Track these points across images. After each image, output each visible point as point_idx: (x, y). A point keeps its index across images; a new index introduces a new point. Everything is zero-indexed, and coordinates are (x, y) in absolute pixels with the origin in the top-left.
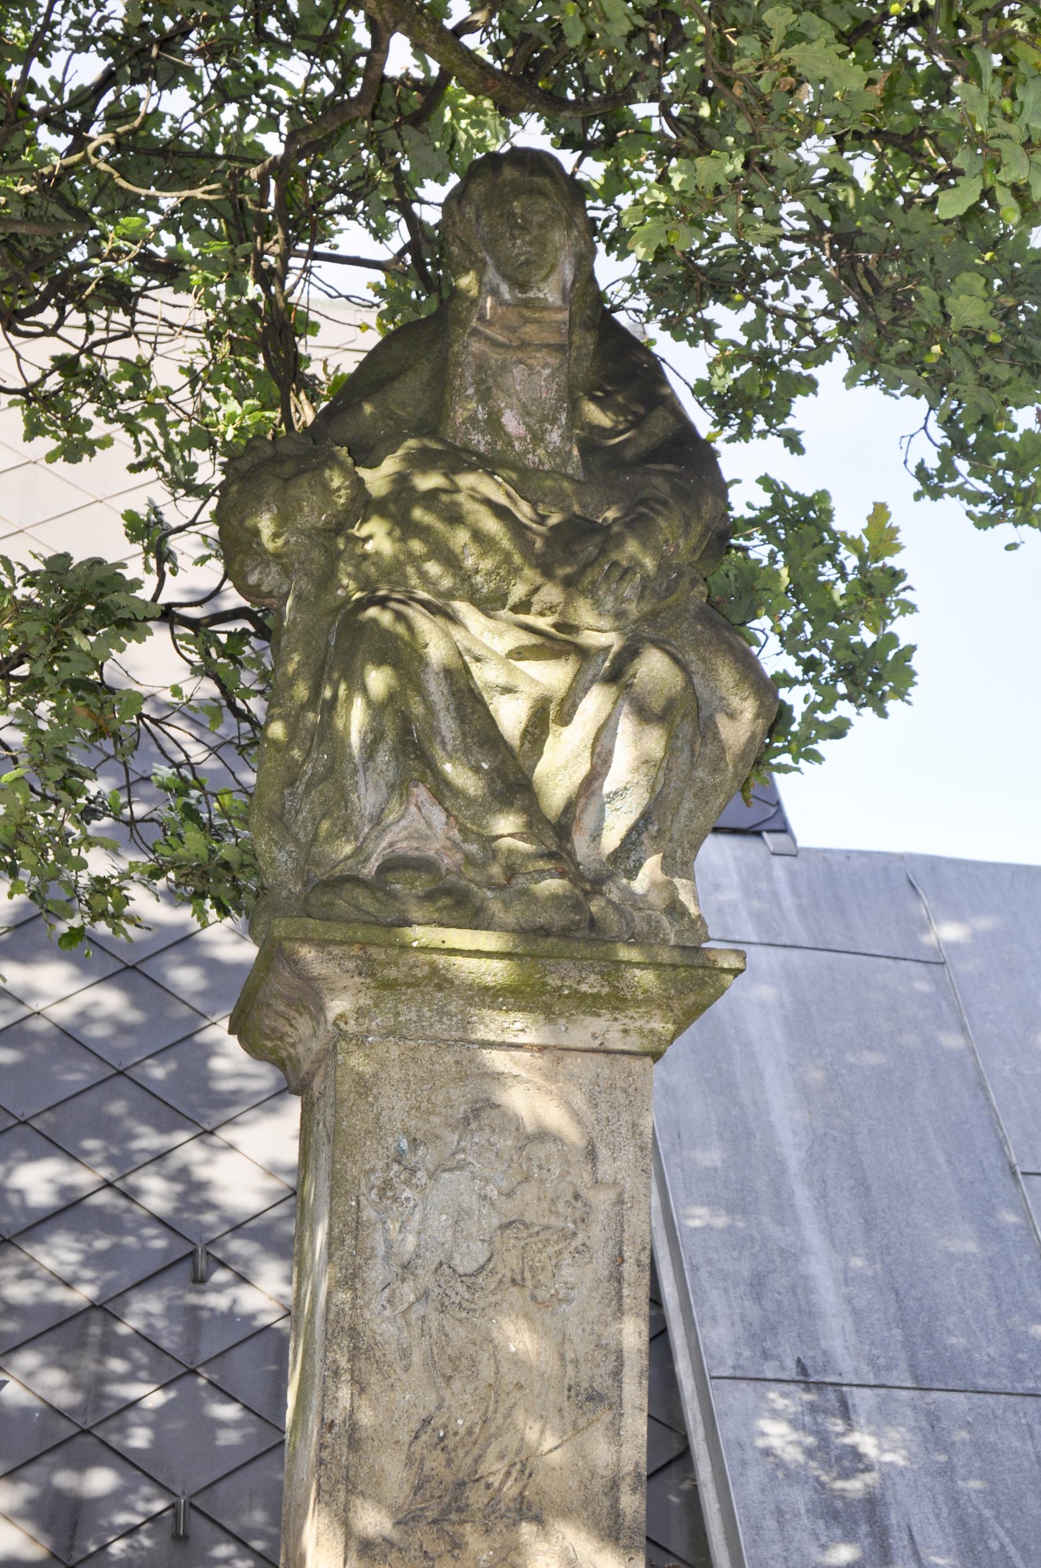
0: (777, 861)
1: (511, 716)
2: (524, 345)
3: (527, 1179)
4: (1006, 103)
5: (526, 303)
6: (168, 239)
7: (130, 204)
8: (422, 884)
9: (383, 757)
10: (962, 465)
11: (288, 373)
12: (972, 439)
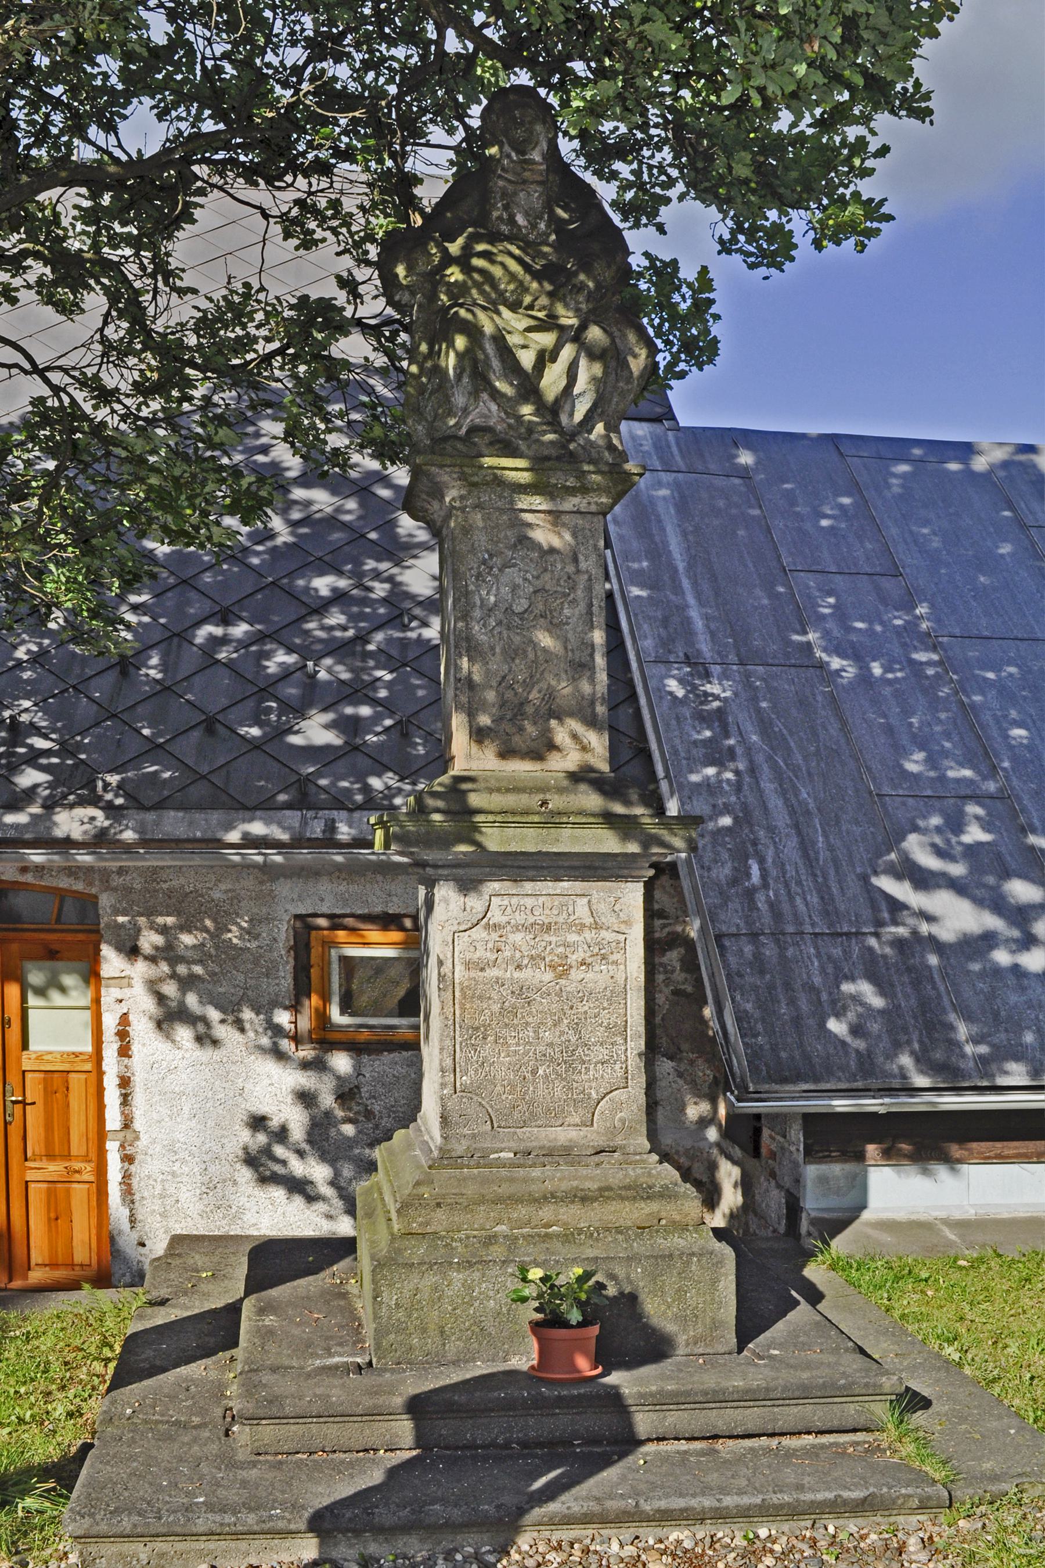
0: (670, 433)
1: (527, 359)
2: (525, 182)
3: (546, 570)
4: (753, 46)
5: (526, 161)
6: (345, 139)
7: (325, 122)
8: (488, 438)
9: (466, 380)
10: (742, 238)
11: (411, 202)
12: (746, 225)
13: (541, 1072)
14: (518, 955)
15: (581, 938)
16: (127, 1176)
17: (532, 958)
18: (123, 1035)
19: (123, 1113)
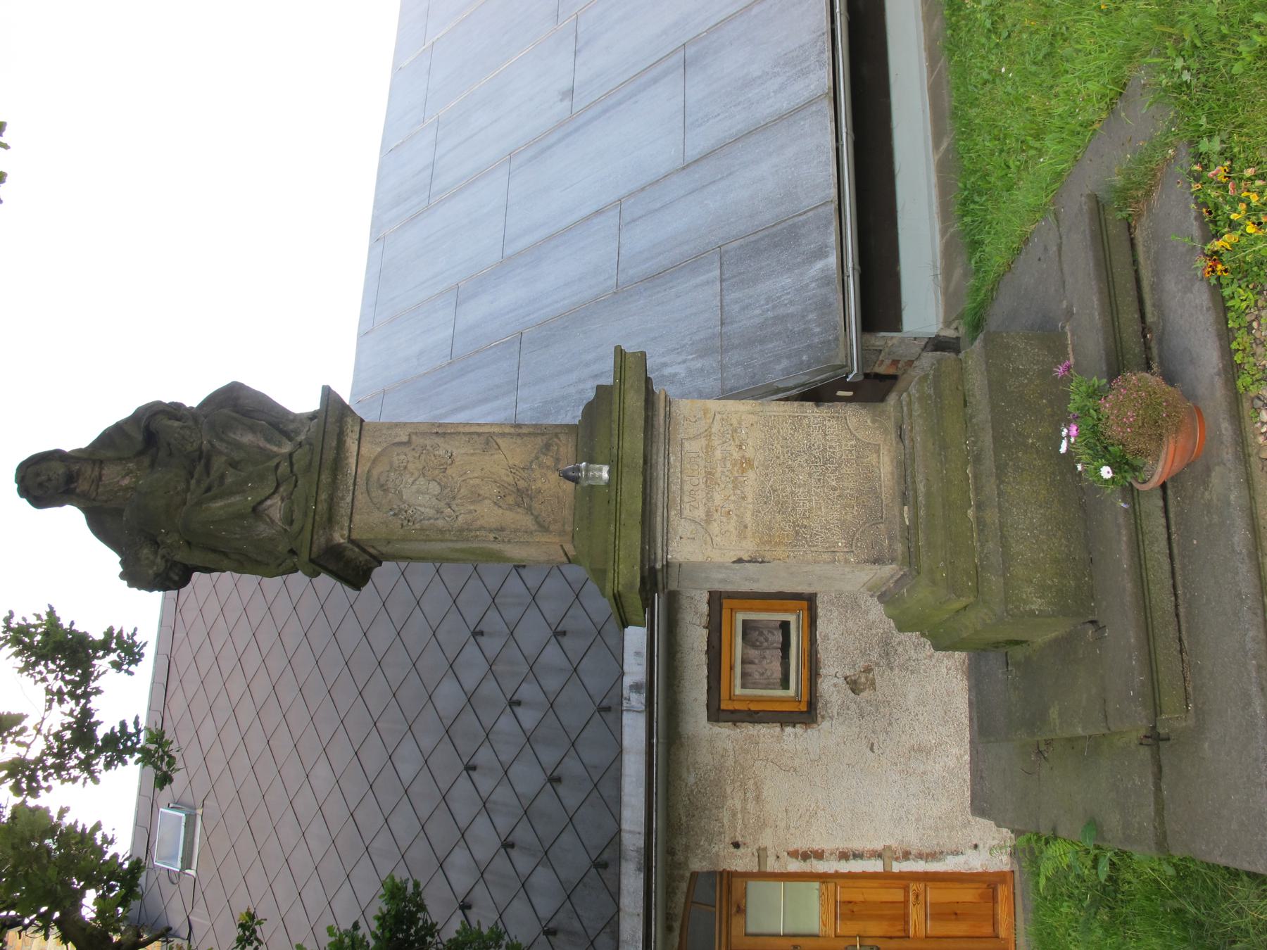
14: (733, 498)
16: (920, 856)
17: (735, 488)
18: (805, 856)
19: (869, 858)
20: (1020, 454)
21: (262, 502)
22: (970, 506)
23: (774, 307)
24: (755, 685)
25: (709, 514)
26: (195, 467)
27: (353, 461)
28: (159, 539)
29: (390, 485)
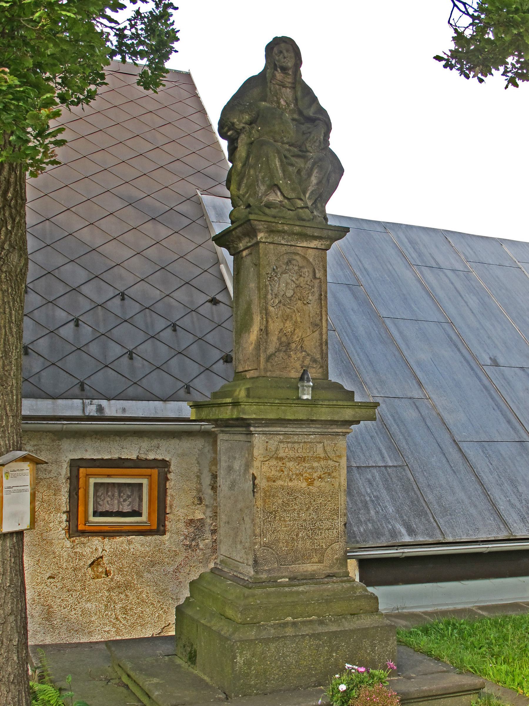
13: (300, 535)
14: (291, 473)
15: (319, 465)
17: (297, 475)
20: (326, 648)
21: (280, 189)
22: (294, 619)
23: (372, 501)
24: (96, 491)
25: (281, 459)
26: (296, 147)
27: (305, 244)
28: (253, 125)
29: (291, 267)
